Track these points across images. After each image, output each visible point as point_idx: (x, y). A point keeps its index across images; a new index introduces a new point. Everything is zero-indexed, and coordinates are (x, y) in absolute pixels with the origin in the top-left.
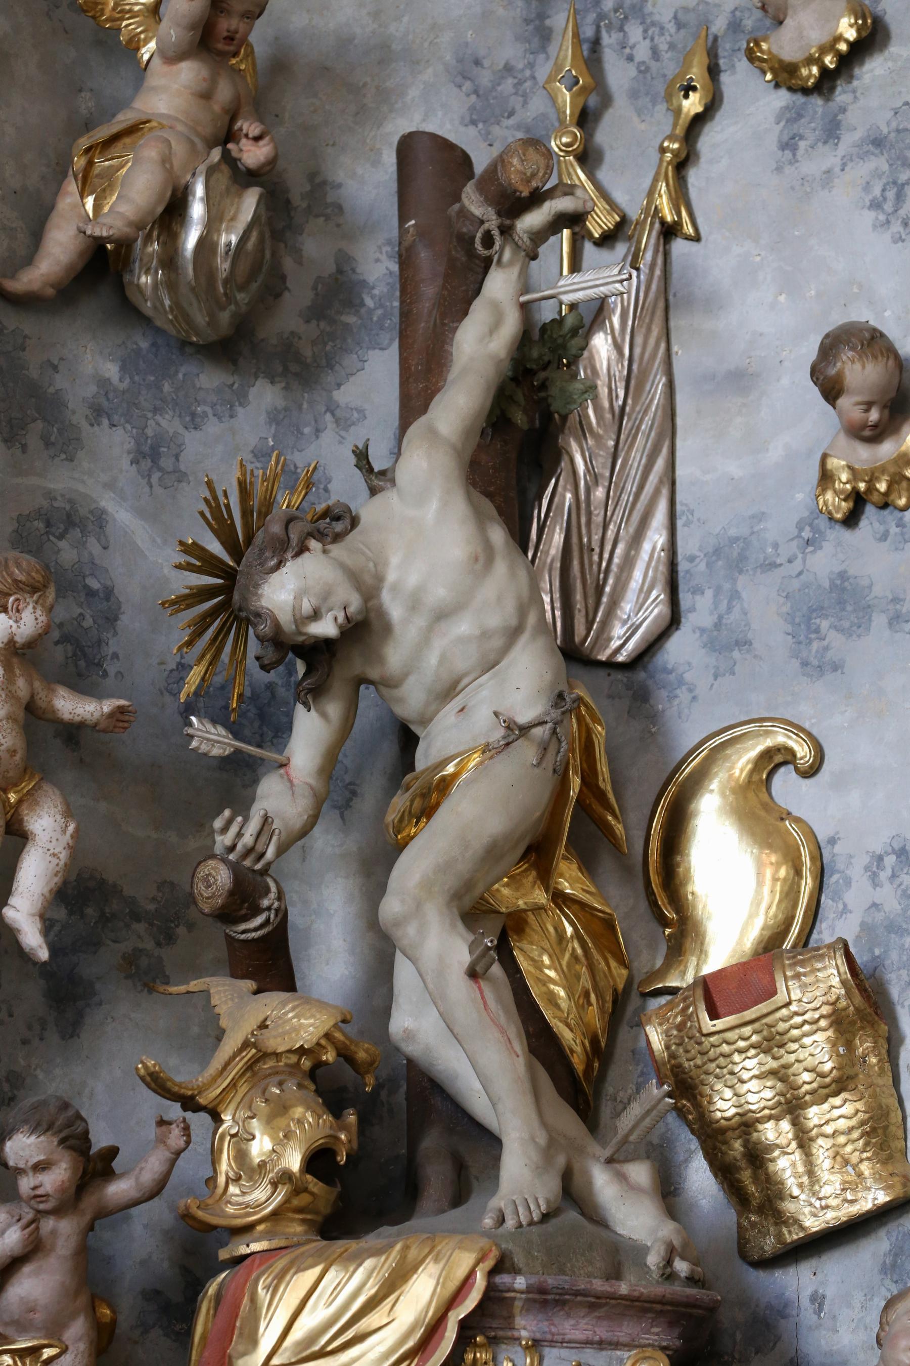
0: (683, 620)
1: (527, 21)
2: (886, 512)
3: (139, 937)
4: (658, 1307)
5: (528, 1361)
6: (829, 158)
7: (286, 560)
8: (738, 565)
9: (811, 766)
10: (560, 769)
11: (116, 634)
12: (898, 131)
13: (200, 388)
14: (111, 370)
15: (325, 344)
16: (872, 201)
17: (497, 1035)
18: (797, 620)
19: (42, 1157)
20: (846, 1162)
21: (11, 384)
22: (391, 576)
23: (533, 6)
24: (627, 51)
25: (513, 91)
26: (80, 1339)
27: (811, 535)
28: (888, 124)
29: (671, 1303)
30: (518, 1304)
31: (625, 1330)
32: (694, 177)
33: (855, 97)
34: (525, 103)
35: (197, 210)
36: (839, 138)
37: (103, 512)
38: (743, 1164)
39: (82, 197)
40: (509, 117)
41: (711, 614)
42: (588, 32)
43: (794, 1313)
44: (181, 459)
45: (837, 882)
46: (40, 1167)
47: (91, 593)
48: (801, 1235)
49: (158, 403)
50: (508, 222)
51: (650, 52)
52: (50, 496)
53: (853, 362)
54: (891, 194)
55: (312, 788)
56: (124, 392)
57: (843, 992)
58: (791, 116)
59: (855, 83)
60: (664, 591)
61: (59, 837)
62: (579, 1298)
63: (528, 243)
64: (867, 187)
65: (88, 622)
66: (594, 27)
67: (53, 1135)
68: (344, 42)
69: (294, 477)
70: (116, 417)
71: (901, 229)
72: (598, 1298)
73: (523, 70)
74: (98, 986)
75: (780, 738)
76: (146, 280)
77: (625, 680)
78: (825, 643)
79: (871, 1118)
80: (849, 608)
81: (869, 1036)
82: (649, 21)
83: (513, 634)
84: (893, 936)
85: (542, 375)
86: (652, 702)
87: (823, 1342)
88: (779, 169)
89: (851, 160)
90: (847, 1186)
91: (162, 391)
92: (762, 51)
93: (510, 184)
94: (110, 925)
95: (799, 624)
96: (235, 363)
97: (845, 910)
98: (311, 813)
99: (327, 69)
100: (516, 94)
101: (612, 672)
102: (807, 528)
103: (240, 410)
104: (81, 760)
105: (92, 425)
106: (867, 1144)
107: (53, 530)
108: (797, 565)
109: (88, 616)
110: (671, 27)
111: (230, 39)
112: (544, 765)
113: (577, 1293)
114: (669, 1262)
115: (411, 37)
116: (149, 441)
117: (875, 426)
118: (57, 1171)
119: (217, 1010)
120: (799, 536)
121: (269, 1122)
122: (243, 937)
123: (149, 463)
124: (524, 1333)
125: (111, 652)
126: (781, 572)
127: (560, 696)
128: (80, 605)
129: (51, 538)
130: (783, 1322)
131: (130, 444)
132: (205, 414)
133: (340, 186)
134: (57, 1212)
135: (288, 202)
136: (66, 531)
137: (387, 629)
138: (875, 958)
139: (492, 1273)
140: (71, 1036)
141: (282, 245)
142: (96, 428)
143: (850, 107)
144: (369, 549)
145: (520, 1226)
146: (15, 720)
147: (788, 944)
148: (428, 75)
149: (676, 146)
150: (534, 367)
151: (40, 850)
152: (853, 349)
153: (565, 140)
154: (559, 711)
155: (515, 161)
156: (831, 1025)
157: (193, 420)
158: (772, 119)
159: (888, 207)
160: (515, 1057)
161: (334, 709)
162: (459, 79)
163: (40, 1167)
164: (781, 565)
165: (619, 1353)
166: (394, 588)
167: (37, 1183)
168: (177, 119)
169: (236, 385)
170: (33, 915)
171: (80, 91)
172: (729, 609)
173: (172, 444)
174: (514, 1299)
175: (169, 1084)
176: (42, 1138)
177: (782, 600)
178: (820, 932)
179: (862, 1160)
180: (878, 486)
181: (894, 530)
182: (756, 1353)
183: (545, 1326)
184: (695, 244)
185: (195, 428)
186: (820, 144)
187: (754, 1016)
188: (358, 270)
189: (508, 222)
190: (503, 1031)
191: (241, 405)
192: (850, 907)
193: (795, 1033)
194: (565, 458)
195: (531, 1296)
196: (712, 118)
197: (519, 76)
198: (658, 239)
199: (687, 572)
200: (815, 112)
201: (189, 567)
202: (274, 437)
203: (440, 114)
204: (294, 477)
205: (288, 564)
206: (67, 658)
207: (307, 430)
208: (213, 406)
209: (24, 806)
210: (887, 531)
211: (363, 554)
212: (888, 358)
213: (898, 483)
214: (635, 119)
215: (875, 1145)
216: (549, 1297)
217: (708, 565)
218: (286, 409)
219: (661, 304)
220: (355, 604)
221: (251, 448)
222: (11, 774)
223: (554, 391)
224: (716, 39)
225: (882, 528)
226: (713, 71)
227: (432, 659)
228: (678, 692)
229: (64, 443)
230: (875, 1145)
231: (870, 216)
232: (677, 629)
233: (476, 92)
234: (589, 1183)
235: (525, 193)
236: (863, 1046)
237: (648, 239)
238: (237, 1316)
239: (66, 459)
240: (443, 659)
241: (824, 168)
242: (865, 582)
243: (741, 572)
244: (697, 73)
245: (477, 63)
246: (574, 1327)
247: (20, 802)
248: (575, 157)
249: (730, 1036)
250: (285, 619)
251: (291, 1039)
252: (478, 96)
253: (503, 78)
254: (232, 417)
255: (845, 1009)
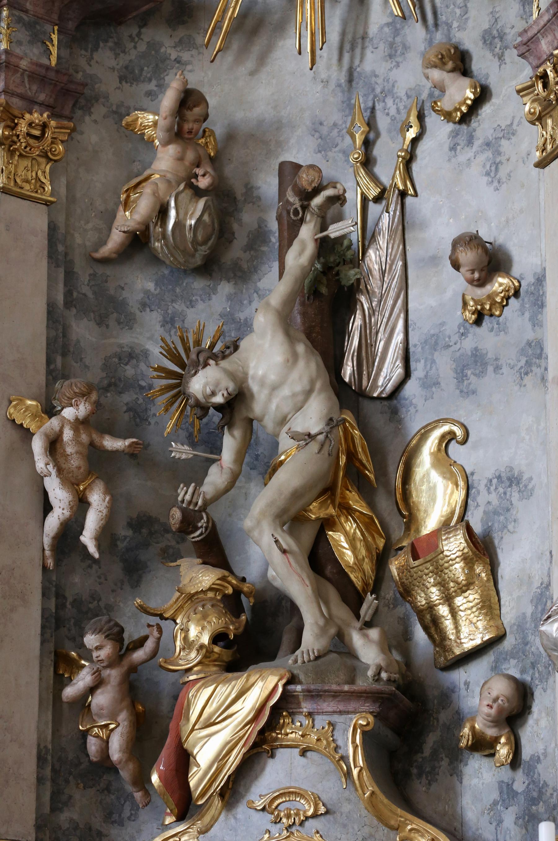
0: (412, 375)
1: (343, 102)
2: (492, 318)
3: (168, 540)
4: (365, 695)
5: (307, 722)
6: (469, 153)
7: (199, 370)
8: (434, 347)
9: (463, 439)
10: (334, 453)
11: (154, 405)
12: (496, 139)
13: (194, 289)
14: (151, 286)
15: (253, 261)
16: (486, 172)
17: (297, 577)
18: (458, 371)
19: (98, 644)
20: (471, 622)
21: (100, 299)
22: (251, 372)
23: (346, 95)
24: (387, 111)
25: (337, 135)
26: (125, 720)
27: (463, 331)
28: (492, 136)
29: (375, 693)
30: (301, 698)
31: (351, 706)
32: (415, 167)
33: (479, 124)
34: (343, 140)
35: (173, 213)
36: (473, 144)
37: (147, 350)
38: (431, 625)
39: (125, 212)
40: (335, 147)
41: (423, 371)
42: (370, 104)
43: (458, 690)
44: (185, 322)
45: (474, 493)
46: (98, 648)
47: (142, 388)
48: (453, 656)
49: (174, 298)
50: (306, 203)
51: (396, 110)
52: (121, 346)
53: (462, 252)
54: (493, 168)
55: (231, 469)
56: (157, 295)
57: (466, 545)
58: (455, 134)
59: (479, 117)
60: (401, 362)
61: (102, 503)
62: (327, 693)
63: (317, 211)
64: (484, 166)
65: (141, 401)
66: (372, 101)
67: (102, 634)
68: (260, 122)
69: (240, 324)
70: (153, 307)
71: (497, 184)
72: (336, 693)
73: (341, 125)
74: (149, 563)
75: (446, 428)
76: (157, 244)
77: (388, 405)
78: (469, 381)
79: (480, 602)
80: (479, 364)
81: (480, 564)
82: (395, 96)
83: (308, 393)
84: (496, 516)
85: (337, 269)
86: (399, 414)
87: (469, 703)
88: (449, 160)
89: (478, 153)
90: (471, 633)
91: (176, 292)
92: (438, 107)
93: (302, 187)
94: (154, 536)
95: (459, 373)
96: (211, 275)
97: (478, 505)
98: (229, 481)
99: (253, 135)
100: (338, 136)
101: (382, 401)
102: (462, 328)
103: (214, 297)
104: (138, 464)
105: (141, 312)
106: (480, 613)
107: (122, 361)
108: (458, 346)
109: (140, 398)
110: (405, 98)
111: (190, 132)
112: (322, 452)
113: (325, 691)
114: (379, 674)
115: (291, 116)
116: (170, 316)
117: (479, 280)
118: (106, 649)
119: (181, 574)
120: (459, 332)
121: (198, 623)
122: (193, 540)
123: (170, 325)
124: (305, 710)
125: (152, 413)
126: (452, 349)
127: (331, 419)
128: (137, 394)
129: (122, 365)
130: (453, 694)
131: (160, 318)
132: (197, 300)
133: (259, 188)
134: (110, 666)
135: (235, 198)
136: (129, 361)
137: (252, 396)
138: (489, 527)
139: (285, 686)
140: (136, 587)
141: (233, 218)
142: (143, 313)
143: (477, 129)
144: (240, 361)
145: (304, 662)
146: (81, 453)
147: (452, 524)
148: (299, 132)
149: (403, 154)
150: (333, 265)
151: (94, 510)
152: (461, 246)
153: (356, 156)
154: (329, 427)
155: (304, 176)
156: (461, 561)
157: (191, 303)
158: (446, 137)
159: (492, 174)
160: (306, 587)
161: (237, 433)
162: (313, 132)
163: (98, 648)
164: (452, 346)
165: (350, 716)
166: (253, 378)
167: (98, 655)
168: (167, 171)
169: (211, 285)
170: (92, 539)
171: (134, 162)
172: (431, 368)
173: (181, 316)
174: (298, 695)
175: (148, 609)
176: (97, 636)
177: (452, 362)
178: (468, 517)
179: (478, 621)
180: (486, 306)
181: (496, 326)
182: (443, 709)
183: (315, 706)
184: (415, 198)
185: (192, 307)
186: (466, 147)
187: (429, 559)
188: (268, 226)
189: (306, 203)
190: (300, 576)
191: (214, 294)
192: (479, 504)
193: (446, 565)
194: (359, 303)
195: (305, 693)
196: (422, 138)
197: (340, 128)
198: (398, 197)
199: (414, 352)
200: (464, 132)
201: (159, 377)
202: (230, 307)
203: (305, 149)
204: (240, 324)
205: (200, 372)
206: (130, 418)
207: (245, 302)
208: (200, 296)
209: (87, 491)
210: (493, 327)
211: (237, 363)
212: (478, 248)
213: (494, 304)
214: (390, 142)
215: (483, 614)
216: (313, 694)
217: (422, 348)
218: (235, 294)
219: (400, 227)
220: (231, 386)
221: (219, 313)
222: (80, 477)
223: (342, 275)
224: (423, 102)
225: (491, 326)
226: (421, 117)
227: (273, 406)
228: (410, 408)
229: (127, 322)
230: (483, 614)
231: (485, 179)
232: (410, 379)
233: (321, 137)
234: (351, 639)
235: (310, 190)
236: (478, 569)
237: (394, 198)
238: (183, 708)
239: (129, 329)
240: (277, 407)
241: (467, 158)
242: (485, 352)
243: (435, 350)
244: (413, 119)
245: (321, 124)
246: (328, 706)
247: (85, 489)
248: (361, 163)
249: (420, 567)
250: (200, 397)
251: (198, 587)
252: (322, 139)
253: (333, 129)
254: (209, 300)
255: (467, 553)
